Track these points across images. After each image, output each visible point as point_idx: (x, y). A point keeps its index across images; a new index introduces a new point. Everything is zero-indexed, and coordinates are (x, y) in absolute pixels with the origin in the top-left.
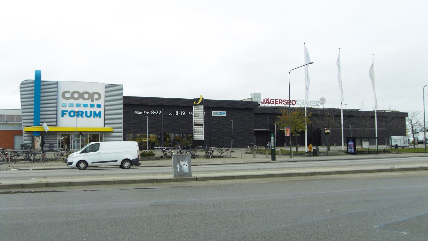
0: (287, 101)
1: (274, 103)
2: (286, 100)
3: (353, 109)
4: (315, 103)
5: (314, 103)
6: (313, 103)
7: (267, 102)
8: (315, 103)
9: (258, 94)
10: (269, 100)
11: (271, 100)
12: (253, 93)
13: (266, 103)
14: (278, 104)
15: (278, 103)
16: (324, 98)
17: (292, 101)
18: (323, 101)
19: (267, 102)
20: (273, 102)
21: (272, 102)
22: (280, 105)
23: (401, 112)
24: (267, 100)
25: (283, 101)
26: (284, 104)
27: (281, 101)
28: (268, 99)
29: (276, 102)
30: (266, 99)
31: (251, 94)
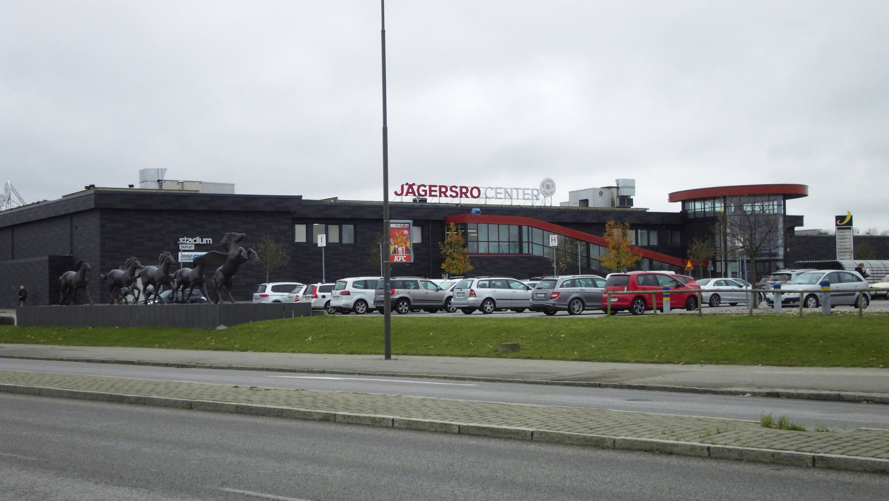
0: (458, 190)
1: (459, 196)
2: (456, 187)
3: (77, 186)
4: (501, 193)
5: (498, 193)
6: (524, 194)
7: (410, 193)
8: (501, 193)
9: (624, 179)
10: (413, 186)
11: (419, 187)
12: (620, 178)
13: (406, 195)
14: (436, 196)
15: (438, 194)
16: (552, 181)
17: (472, 189)
18: (548, 187)
19: (410, 191)
20: (425, 191)
21: (423, 191)
22: (444, 200)
23: (652, 210)
24: (411, 186)
25: (449, 188)
26: (451, 196)
27: (443, 190)
28: (411, 183)
29: (431, 191)
30: (407, 184)
31: (617, 181)
